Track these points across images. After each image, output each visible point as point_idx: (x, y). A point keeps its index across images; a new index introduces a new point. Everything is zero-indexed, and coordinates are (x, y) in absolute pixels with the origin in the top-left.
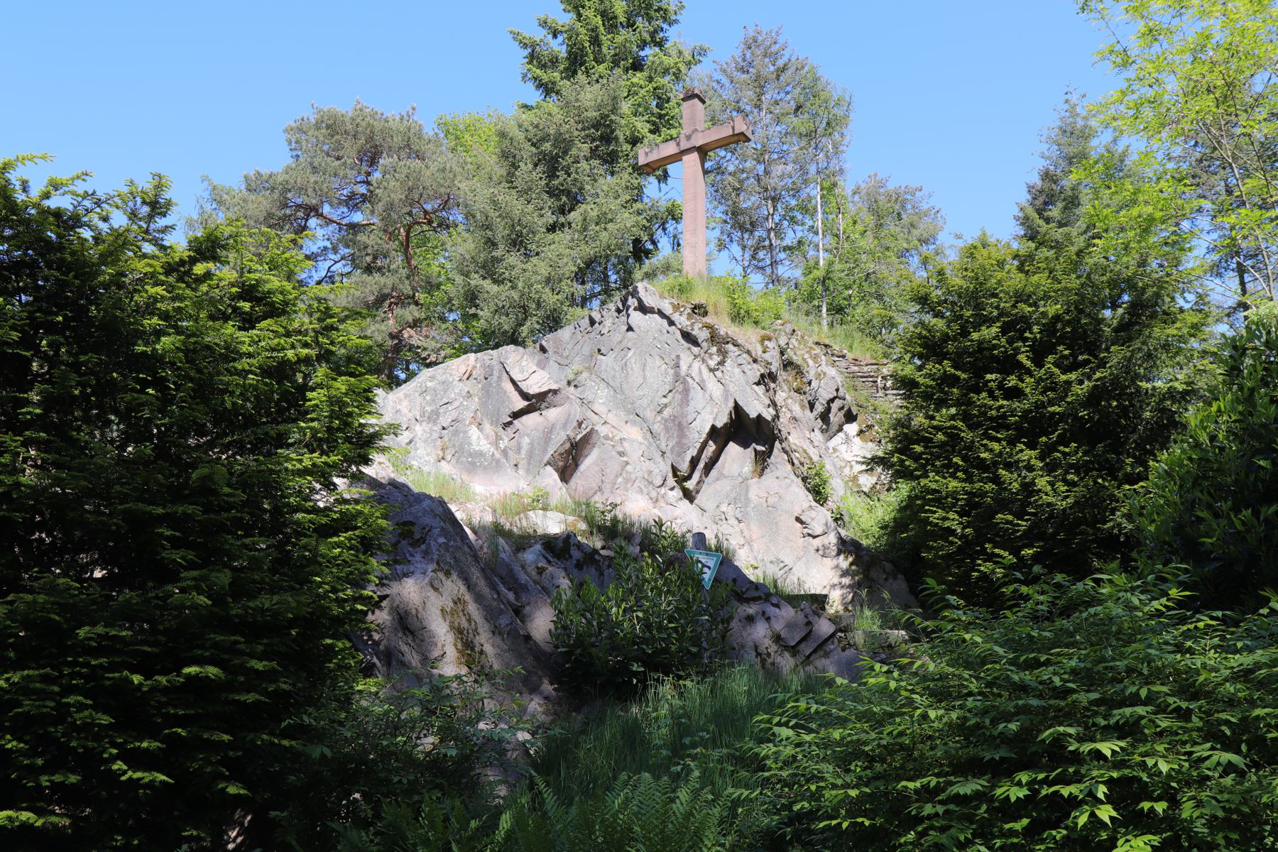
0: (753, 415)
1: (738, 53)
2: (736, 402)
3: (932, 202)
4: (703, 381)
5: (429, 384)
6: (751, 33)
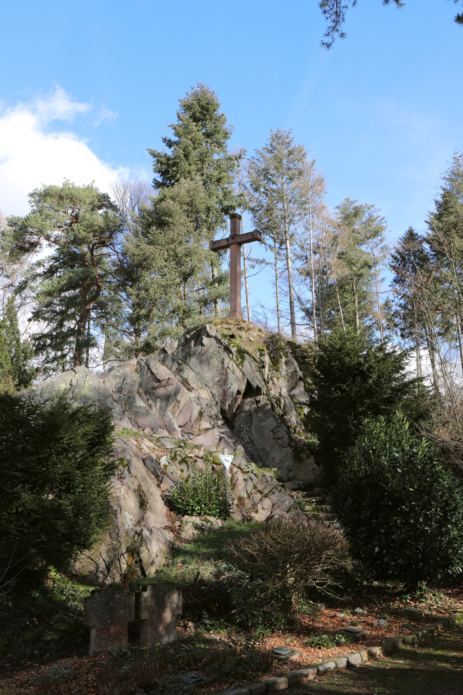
0: (255, 386)
1: (268, 143)
2: (248, 380)
3: (379, 213)
4: (234, 370)
5: (117, 374)
6: (275, 132)
